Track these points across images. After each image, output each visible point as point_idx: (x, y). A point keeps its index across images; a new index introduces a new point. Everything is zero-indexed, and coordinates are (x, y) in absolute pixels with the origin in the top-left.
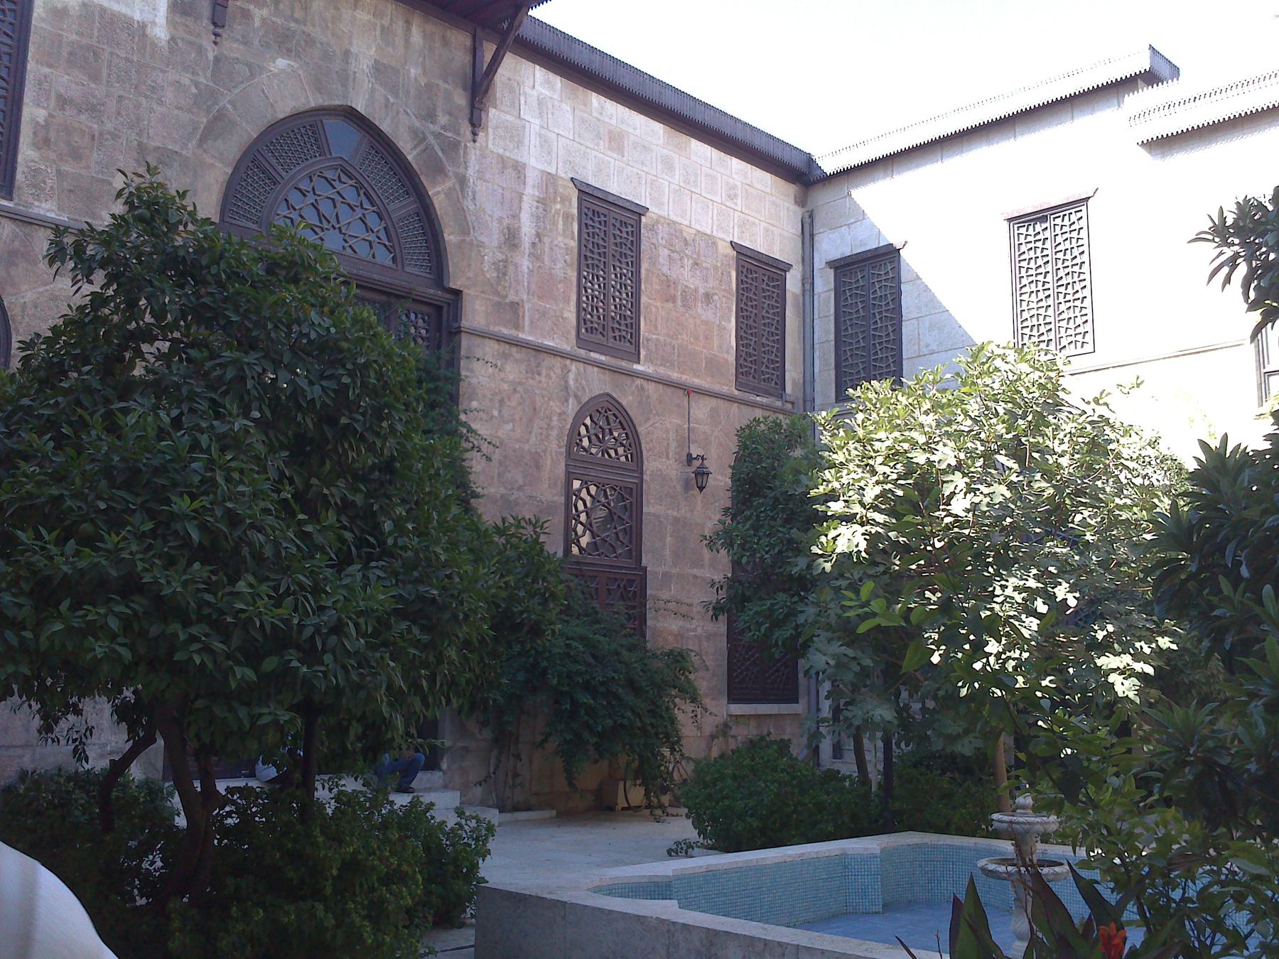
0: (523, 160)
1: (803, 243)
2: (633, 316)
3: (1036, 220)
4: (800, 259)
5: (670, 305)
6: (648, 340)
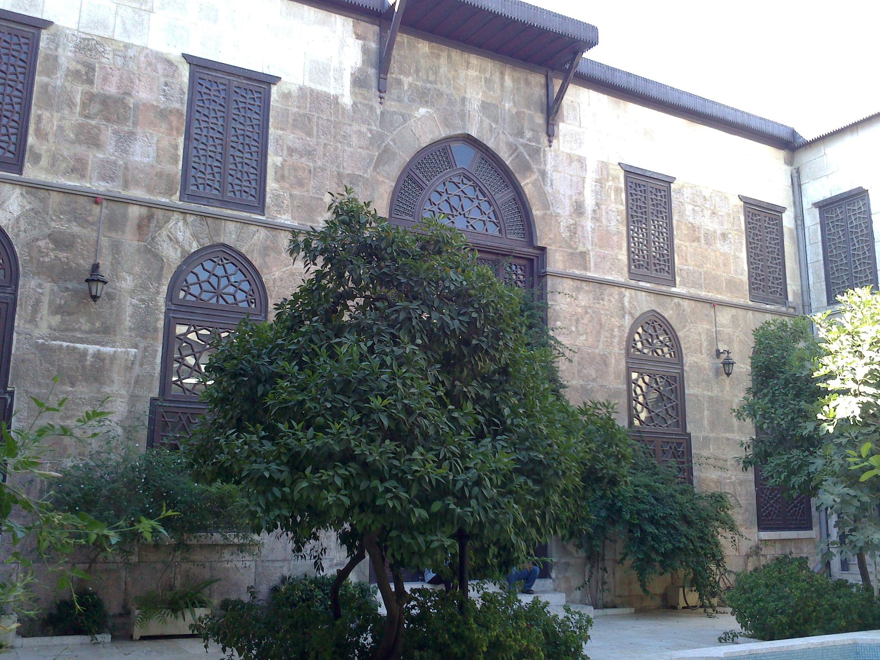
2: (669, 254)
6: (681, 270)
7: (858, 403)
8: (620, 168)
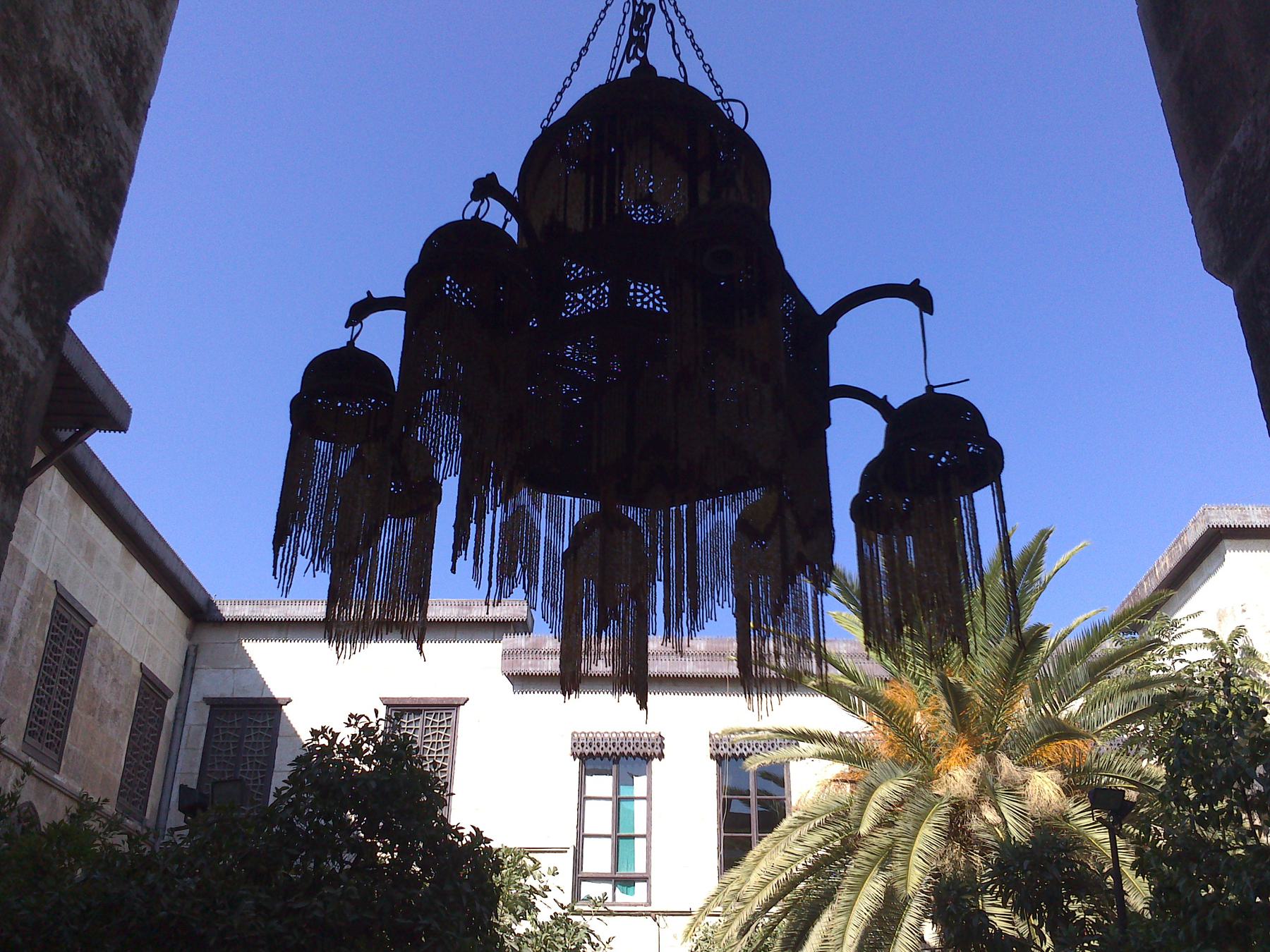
0: (28, 555)
1: (184, 675)
2: (64, 724)
3: (410, 712)
4: (178, 690)
5: (90, 717)
6: (69, 750)
7: (818, 785)
8: (54, 588)
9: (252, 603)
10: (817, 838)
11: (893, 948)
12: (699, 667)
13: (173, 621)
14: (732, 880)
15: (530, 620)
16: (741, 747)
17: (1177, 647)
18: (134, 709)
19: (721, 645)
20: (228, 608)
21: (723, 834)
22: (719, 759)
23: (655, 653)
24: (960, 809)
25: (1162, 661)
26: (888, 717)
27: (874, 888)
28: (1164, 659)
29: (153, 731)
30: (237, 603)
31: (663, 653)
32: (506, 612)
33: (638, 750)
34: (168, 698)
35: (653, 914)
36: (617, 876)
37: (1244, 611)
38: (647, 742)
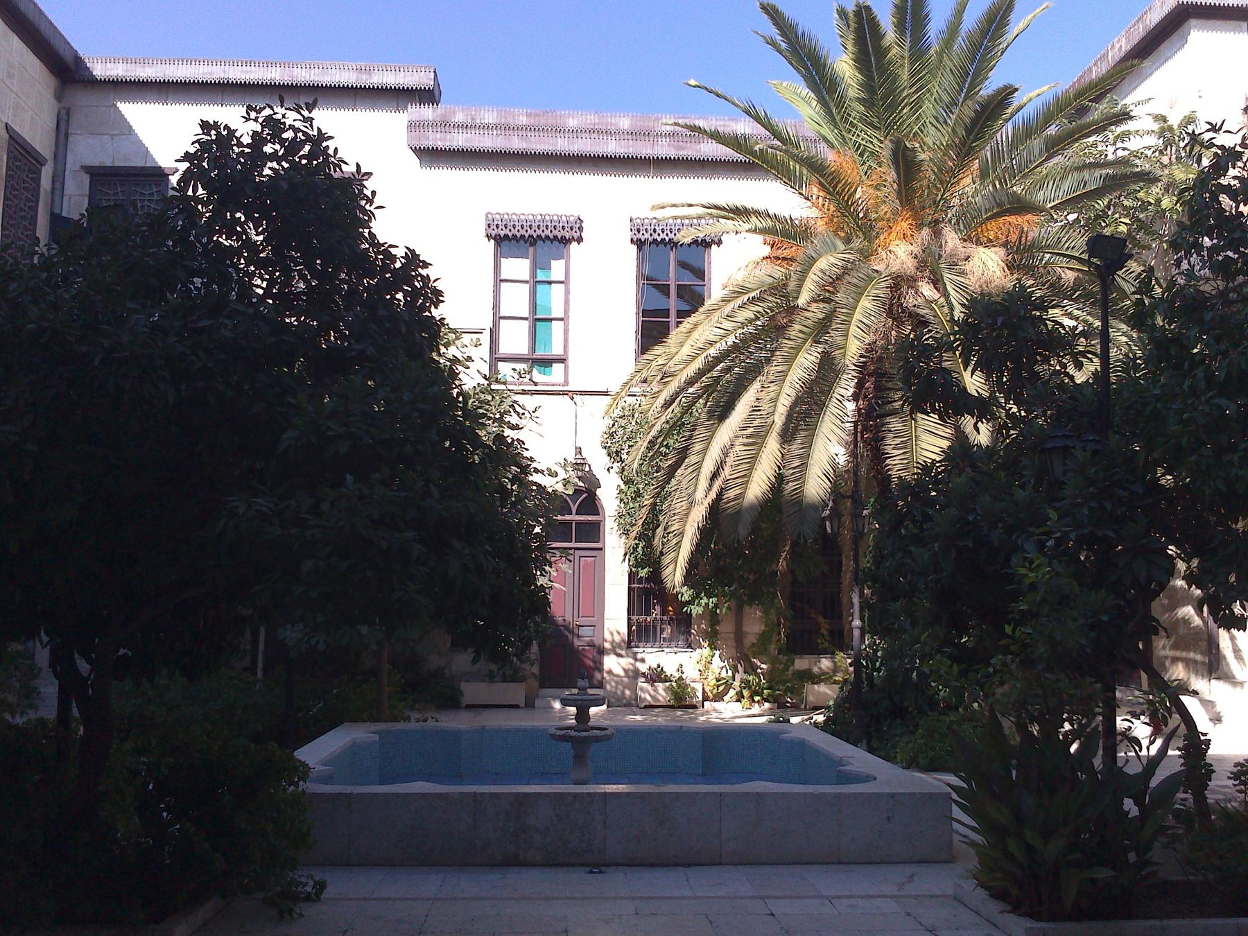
4: (53, 156)
9: (126, 61)
10: (747, 314)
11: (823, 418)
12: (621, 147)
13: (37, 78)
14: (655, 357)
15: (436, 89)
16: (663, 232)
17: (1123, 133)
18: (4, 174)
19: (646, 124)
20: (99, 67)
21: (641, 319)
22: (640, 244)
23: (575, 130)
24: (899, 283)
25: (1104, 148)
26: (831, 190)
27: (808, 359)
28: (1107, 146)
29: (29, 200)
30: (108, 61)
31: (584, 130)
32: (410, 79)
33: (556, 233)
34: (42, 165)
35: (570, 394)
36: (534, 357)
37: (1200, 97)
38: (566, 225)
